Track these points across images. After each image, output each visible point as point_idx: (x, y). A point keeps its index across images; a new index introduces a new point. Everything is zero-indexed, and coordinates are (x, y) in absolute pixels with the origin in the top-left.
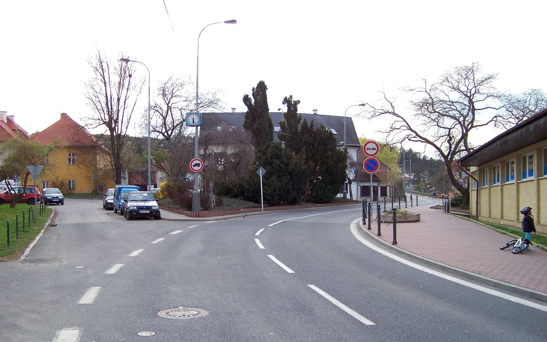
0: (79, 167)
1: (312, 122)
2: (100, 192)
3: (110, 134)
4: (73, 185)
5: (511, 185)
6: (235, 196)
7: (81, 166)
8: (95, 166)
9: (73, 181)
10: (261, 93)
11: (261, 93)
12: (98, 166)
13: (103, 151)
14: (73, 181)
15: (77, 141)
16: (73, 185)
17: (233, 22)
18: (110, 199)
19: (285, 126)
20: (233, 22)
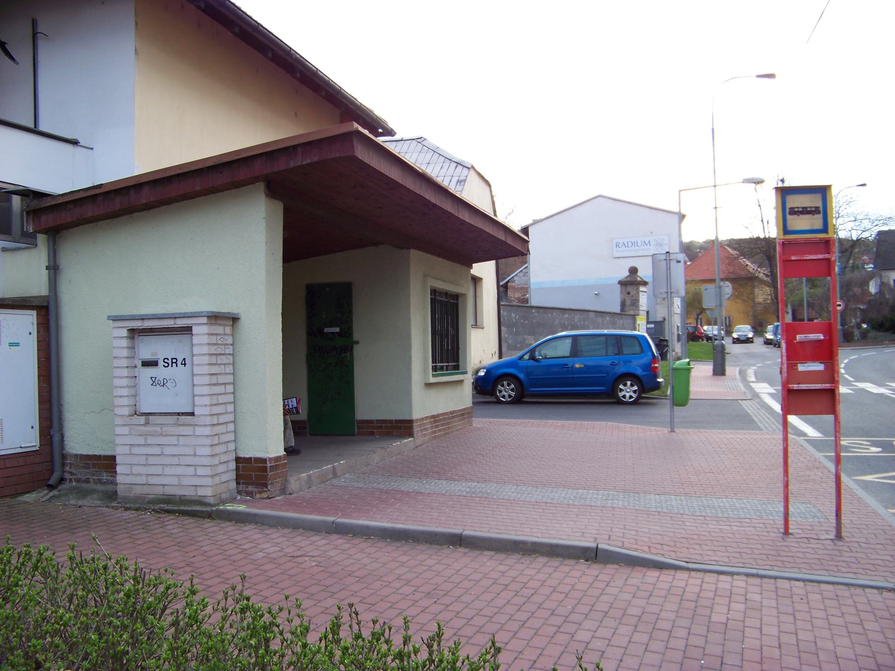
0: (736, 302)
1: (131, 416)
2: (759, 329)
3: (494, 261)
4: (730, 321)
5: (569, 211)
6: (887, 330)
7: (738, 301)
8: (753, 301)
9: (729, 317)
10: (702, 662)
11: (702, 662)
12: (756, 300)
13: (762, 282)
14: (729, 317)
15: (732, 273)
16: (730, 321)
17: (864, 185)
18: (769, 336)
19: (454, 365)
20: (864, 185)
